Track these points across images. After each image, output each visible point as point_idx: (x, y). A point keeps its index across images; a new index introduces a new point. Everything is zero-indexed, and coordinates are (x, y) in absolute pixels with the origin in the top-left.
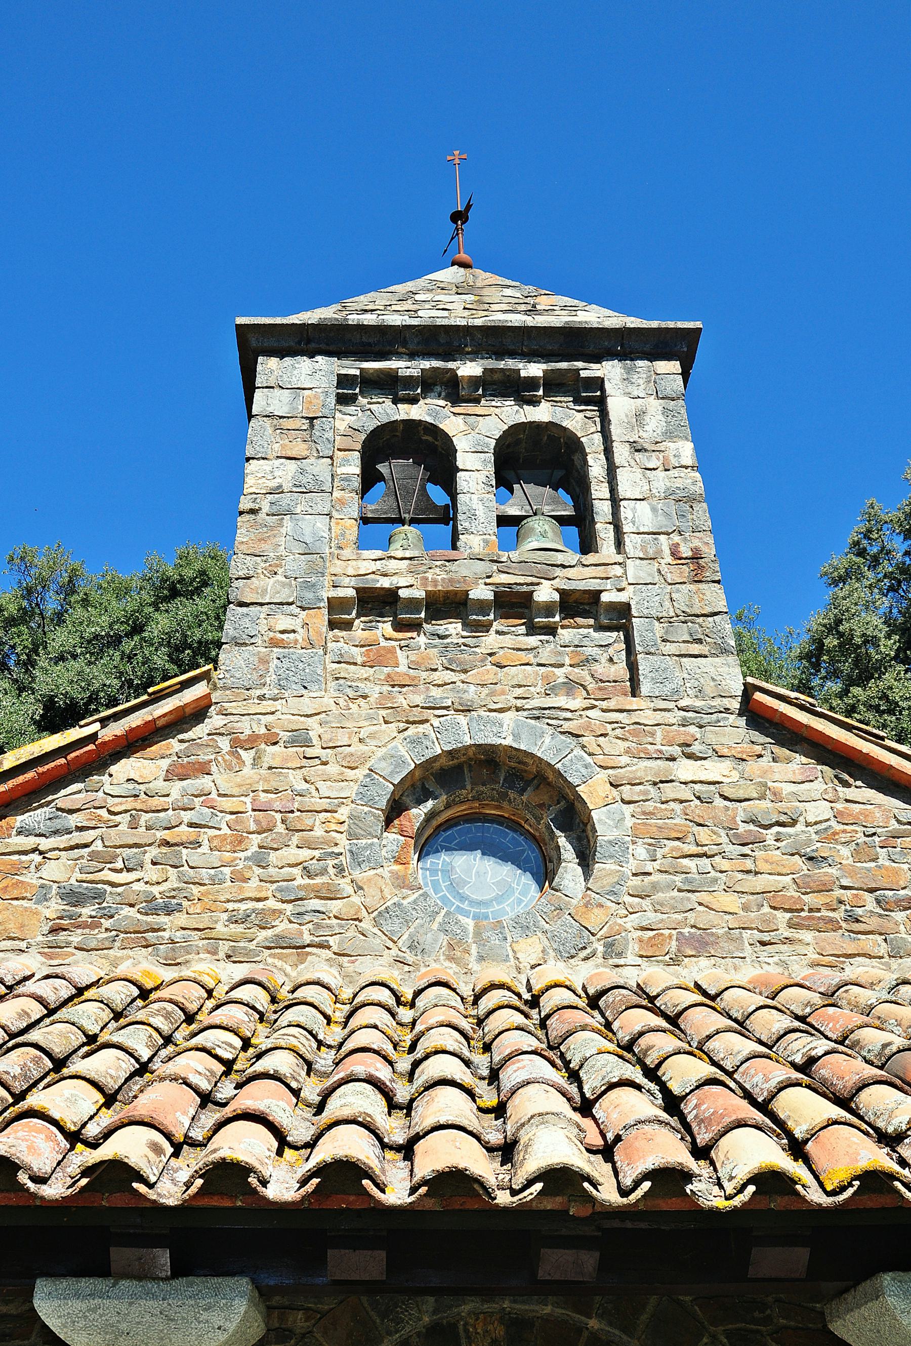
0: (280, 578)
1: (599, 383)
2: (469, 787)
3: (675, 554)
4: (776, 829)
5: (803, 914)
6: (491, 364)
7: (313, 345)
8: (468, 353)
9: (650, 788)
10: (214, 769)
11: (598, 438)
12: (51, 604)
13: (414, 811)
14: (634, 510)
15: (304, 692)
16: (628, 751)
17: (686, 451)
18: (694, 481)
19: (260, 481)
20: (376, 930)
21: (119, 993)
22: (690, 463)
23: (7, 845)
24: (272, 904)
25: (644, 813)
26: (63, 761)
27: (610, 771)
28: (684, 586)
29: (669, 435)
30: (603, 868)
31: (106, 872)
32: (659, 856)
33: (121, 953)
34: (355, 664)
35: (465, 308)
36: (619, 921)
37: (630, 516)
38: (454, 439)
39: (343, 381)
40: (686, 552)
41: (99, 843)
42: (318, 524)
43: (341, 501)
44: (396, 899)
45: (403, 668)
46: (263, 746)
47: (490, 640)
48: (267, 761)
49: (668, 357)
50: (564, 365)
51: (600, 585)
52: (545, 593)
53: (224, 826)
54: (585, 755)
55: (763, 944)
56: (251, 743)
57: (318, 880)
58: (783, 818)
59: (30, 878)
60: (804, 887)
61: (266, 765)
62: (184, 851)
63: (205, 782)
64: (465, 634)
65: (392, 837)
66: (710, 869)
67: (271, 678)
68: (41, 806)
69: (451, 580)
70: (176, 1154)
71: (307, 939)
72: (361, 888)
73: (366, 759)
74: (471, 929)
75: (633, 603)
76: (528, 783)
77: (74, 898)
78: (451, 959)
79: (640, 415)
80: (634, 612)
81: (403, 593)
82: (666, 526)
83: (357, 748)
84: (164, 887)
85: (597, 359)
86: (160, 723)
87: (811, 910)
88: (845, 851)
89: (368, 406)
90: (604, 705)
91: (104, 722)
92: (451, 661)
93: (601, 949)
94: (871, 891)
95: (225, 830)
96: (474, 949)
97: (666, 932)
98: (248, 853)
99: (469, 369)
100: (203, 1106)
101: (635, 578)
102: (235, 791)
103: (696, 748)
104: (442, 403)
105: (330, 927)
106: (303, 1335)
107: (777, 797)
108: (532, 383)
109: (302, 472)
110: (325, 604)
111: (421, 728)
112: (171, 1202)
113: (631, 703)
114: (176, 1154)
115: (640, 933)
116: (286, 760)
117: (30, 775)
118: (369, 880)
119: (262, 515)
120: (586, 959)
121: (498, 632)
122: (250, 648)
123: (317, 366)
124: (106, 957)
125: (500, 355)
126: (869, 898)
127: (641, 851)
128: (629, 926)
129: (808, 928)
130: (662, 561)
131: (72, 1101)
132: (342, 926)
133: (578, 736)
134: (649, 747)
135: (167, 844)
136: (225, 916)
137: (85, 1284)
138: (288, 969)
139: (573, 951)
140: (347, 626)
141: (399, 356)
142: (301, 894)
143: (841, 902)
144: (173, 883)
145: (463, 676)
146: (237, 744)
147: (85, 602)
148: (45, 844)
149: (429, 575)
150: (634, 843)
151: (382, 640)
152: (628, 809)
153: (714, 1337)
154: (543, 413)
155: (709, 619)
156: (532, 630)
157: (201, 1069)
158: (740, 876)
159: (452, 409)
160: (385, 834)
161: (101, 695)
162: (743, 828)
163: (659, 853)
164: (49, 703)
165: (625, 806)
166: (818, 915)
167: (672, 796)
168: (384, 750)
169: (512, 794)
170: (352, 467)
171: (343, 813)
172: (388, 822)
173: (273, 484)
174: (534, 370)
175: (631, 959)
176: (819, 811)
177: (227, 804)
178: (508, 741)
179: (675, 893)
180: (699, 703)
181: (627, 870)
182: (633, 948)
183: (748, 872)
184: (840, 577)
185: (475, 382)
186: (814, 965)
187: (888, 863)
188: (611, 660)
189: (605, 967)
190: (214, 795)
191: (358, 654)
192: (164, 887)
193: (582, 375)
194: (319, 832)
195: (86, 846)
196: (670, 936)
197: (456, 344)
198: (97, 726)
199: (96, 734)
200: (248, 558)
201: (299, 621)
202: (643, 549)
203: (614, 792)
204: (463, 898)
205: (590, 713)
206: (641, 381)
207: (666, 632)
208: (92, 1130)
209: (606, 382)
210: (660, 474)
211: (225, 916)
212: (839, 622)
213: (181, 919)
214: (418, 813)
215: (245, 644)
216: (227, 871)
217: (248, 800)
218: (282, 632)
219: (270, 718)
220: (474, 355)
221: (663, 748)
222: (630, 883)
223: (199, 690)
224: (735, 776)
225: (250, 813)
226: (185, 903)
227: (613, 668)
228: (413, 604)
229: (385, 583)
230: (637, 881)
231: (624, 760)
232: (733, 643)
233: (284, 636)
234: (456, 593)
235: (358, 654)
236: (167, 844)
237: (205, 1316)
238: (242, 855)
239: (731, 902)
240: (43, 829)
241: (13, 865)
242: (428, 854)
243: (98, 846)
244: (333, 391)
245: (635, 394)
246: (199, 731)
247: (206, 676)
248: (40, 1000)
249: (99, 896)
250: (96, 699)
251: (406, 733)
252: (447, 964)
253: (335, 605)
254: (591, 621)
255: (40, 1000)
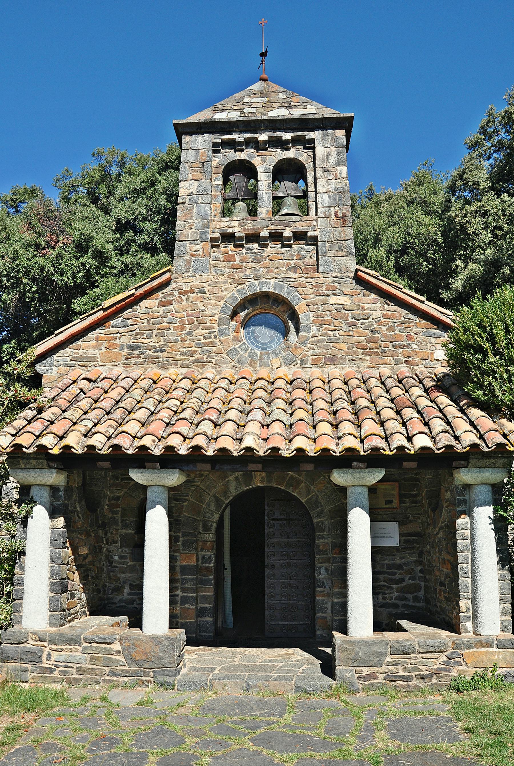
0: (193, 230)
1: (313, 141)
2: (260, 305)
3: (336, 216)
4: (362, 321)
5: (367, 350)
6: (271, 134)
7: (203, 130)
8: (263, 130)
9: (320, 306)
10: (173, 303)
11: (312, 164)
12: (114, 170)
13: (241, 314)
14: (322, 197)
15: (203, 274)
16: (313, 293)
17: (344, 170)
18: (346, 184)
19: (185, 191)
20: (227, 357)
21: (145, 384)
22: (345, 176)
23: (109, 331)
24: (194, 349)
25: (317, 315)
26: (124, 303)
27: (307, 300)
28: (338, 229)
29: (338, 164)
30: (302, 334)
31: (141, 339)
32: (321, 330)
33: (147, 366)
34: (221, 261)
35: (263, 107)
36: (306, 353)
37: (320, 200)
38: (257, 167)
39: (215, 144)
40: (340, 214)
41: (138, 329)
42: (206, 208)
43: (215, 196)
44: (233, 346)
45: (237, 262)
46: (189, 294)
47: (268, 250)
48: (191, 300)
49: (341, 129)
50: (299, 134)
51: (307, 229)
52: (287, 233)
53: (178, 323)
54: (298, 295)
55: (353, 360)
56: (185, 293)
57: (209, 341)
58: (364, 317)
59: (117, 342)
60: (369, 340)
61: (190, 301)
62: (165, 332)
63: (171, 307)
64: (259, 248)
65: (233, 323)
66: (338, 335)
67: (191, 269)
68: (119, 317)
69: (254, 229)
70: (159, 441)
71: (205, 360)
72: (222, 343)
73: (223, 298)
74: (259, 355)
75: (319, 236)
76: (280, 303)
77: (132, 348)
78: (251, 366)
79: (328, 155)
80: (319, 240)
81: (237, 235)
82: (334, 204)
83: (221, 294)
84: (160, 344)
85: (312, 130)
86: (154, 288)
87: (370, 349)
88: (384, 328)
89: (225, 154)
90: (306, 276)
91: (136, 289)
92: (254, 259)
93: (299, 362)
94: (391, 342)
95: (178, 324)
96: (258, 363)
97: (321, 356)
98: (186, 332)
99: (263, 137)
100: (167, 426)
101: (320, 226)
102: (181, 310)
103: (337, 291)
104: (253, 151)
105: (213, 356)
106: (207, 476)
107: (363, 309)
108: (287, 142)
109: (200, 186)
110: (209, 240)
111: (242, 286)
112: (157, 454)
113: (315, 275)
114: (159, 441)
115: (313, 357)
116: (197, 299)
117: (114, 308)
118: (225, 340)
119: (186, 205)
120: (294, 365)
121: (271, 247)
122: (184, 258)
123: (205, 139)
124: (143, 367)
125: (275, 130)
126: (390, 345)
127: (315, 329)
128: (309, 355)
129: (368, 355)
130: (331, 219)
131: (133, 428)
132: (216, 356)
133: (296, 288)
134: (320, 291)
135: (160, 329)
136: (179, 353)
137: (140, 470)
138: (200, 370)
139: (290, 363)
140: (218, 246)
141: (236, 132)
142: (203, 345)
143: (380, 346)
144: (162, 342)
145: (258, 265)
146: (180, 293)
147: (130, 173)
148: (121, 330)
149: (246, 227)
150: (313, 326)
151: (230, 251)
152: (311, 314)
153: (324, 477)
154: (291, 154)
155: (347, 242)
156: (283, 246)
157: (167, 415)
158: (347, 337)
159: (257, 154)
160: (231, 322)
161: (140, 216)
162: (350, 320)
163: (321, 329)
164: (118, 221)
165: (310, 313)
166: (372, 350)
167: (327, 309)
168: (230, 294)
169: (274, 307)
170: (219, 182)
171: (216, 317)
172: (232, 318)
173: (190, 192)
174: (288, 136)
175: (309, 365)
176: (377, 314)
177: (178, 315)
178: (272, 290)
179: (325, 343)
180: (339, 275)
181: (310, 335)
182: (310, 362)
183: (350, 336)
184: (472, 145)
185: (265, 142)
186: (369, 367)
187: (398, 333)
188: (311, 257)
189: (300, 368)
190: (174, 312)
191: (221, 257)
192: (160, 344)
193: (307, 138)
194: (208, 324)
195: (134, 331)
196: (322, 358)
197: (258, 127)
198: (134, 290)
199: (134, 293)
200: (182, 222)
201: (200, 247)
202: (325, 214)
203: (308, 308)
204: (258, 342)
205: (301, 279)
206: (329, 140)
207: (330, 248)
208: (139, 435)
209: (316, 141)
210: (334, 181)
211: (179, 353)
212: (464, 173)
213: (165, 354)
214: (243, 314)
215: (182, 257)
216: (179, 338)
217: (185, 313)
218: (195, 251)
219: (191, 284)
220: (265, 131)
221: (325, 292)
222: (310, 340)
223: (167, 276)
224: (350, 301)
225: (186, 318)
226: (166, 349)
227: (311, 260)
228: (240, 239)
229: (230, 231)
230: (313, 339)
231: (312, 296)
232: (354, 251)
233: (195, 253)
234: (256, 233)
235: (221, 257)
236: (160, 329)
237: (169, 477)
238: (184, 332)
239: (344, 346)
240: (120, 326)
241: (111, 338)
242: (247, 327)
243: (138, 331)
244: (211, 149)
245: (327, 145)
246: (168, 290)
247: (169, 270)
248: (124, 388)
249: (139, 347)
250: (137, 218)
251: (238, 288)
252: (250, 367)
253: (213, 240)
254: (304, 242)
255: (124, 388)
